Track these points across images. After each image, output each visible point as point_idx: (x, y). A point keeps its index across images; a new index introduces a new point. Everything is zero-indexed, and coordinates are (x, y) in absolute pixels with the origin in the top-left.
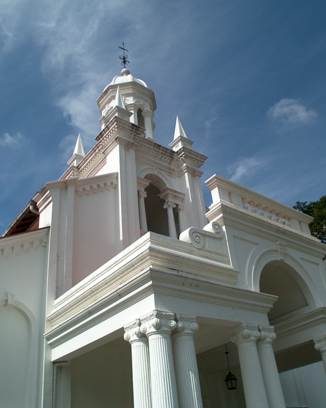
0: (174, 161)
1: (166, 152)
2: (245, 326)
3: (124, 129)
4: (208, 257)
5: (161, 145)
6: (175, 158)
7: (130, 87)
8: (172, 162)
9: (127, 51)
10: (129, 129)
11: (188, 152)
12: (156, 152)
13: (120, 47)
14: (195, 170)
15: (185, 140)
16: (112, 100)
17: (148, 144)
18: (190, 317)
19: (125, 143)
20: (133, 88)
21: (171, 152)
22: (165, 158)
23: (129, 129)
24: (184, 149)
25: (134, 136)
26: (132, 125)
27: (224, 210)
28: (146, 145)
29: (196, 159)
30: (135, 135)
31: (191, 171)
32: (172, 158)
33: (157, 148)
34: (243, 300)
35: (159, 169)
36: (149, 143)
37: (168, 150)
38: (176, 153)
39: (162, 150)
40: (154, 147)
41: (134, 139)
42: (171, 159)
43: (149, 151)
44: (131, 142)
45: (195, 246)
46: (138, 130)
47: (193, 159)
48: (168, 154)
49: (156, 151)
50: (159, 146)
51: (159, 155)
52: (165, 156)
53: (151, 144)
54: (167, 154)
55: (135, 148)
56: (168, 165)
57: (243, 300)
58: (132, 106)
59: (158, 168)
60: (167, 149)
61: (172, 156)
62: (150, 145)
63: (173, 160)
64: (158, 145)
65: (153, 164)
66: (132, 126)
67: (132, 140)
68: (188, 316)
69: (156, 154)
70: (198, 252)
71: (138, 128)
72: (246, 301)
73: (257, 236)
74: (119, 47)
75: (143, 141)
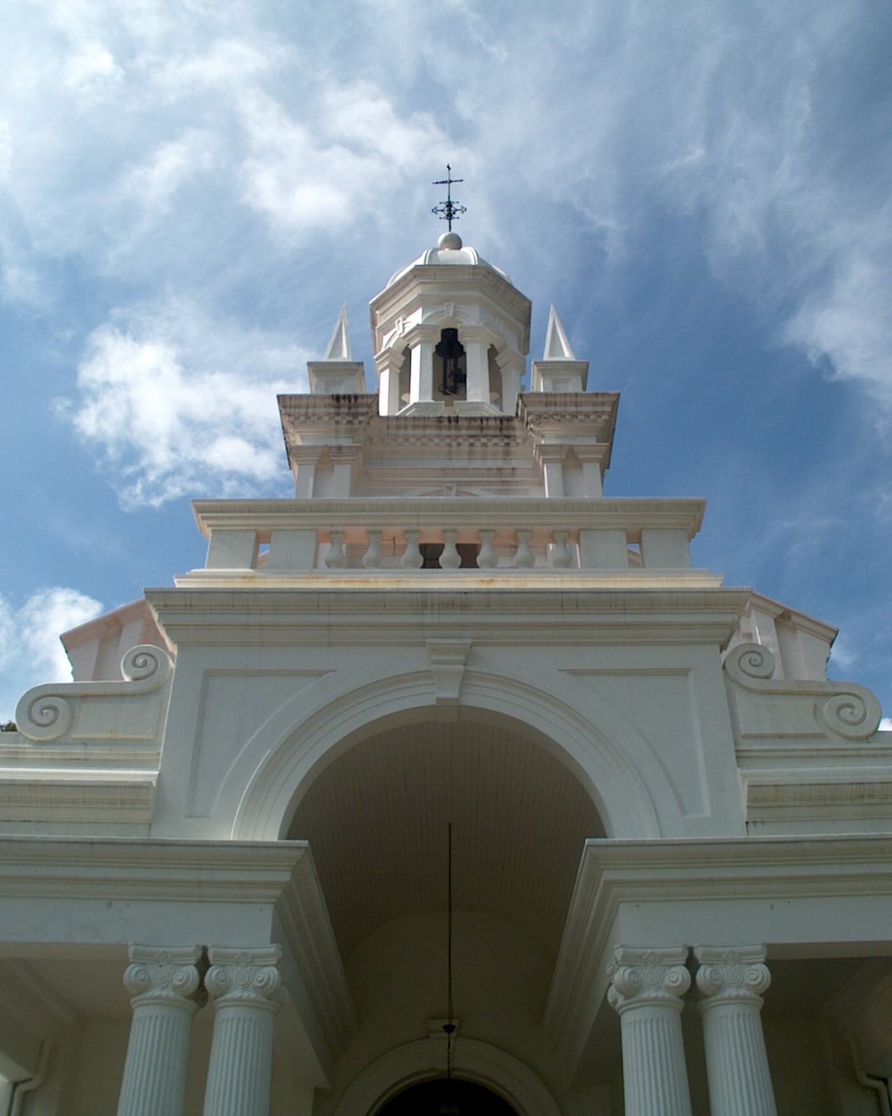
0: (518, 444)
1: (482, 429)
2: (619, 958)
3: (312, 418)
4: (78, 759)
5: (460, 415)
6: (518, 433)
7: (412, 285)
8: (513, 449)
9: (461, 181)
10: (328, 414)
11: (540, 402)
12: (447, 441)
13: (437, 183)
14: (575, 448)
15: (556, 367)
16: (382, 338)
17: (414, 427)
18: (659, 951)
19: (316, 456)
20: (421, 283)
21: (498, 423)
22: (485, 445)
23: (328, 414)
24: (525, 399)
25: (349, 426)
26: (333, 399)
27: (162, 603)
28: (410, 432)
29: (577, 412)
30: (350, 422)
31: (558, 457)
32: (508, 437)
33: (450, 428)
34: (143, 874)
35: (458, 486)
36: (417, 423)
37: (488, 419)
38: (515, 419)
39: (469, 428)
40: (440, 428)
41: (352, 433)
42: (506, 440)
43: (423, 444)
44: (335, 447)
45: (30, 737)
46: (356, 406)
47: (568, 417)
48: (491, 432)
49: (449, 437)
50: (452, 419)
51: (459, 444)
52: (484, 440)
53: (426, 423)
54: (485, 432)
55: (351, 456)
56: (500, 464)
57: (143, 874)
58: (416, 335)
59: (455, 484)
60: (482, 419)
61: (504, 432)
62: (425, 427)
63: (513, 443)
64: (449, 419)
65: (441, 479)
66: (335, 403)
67: (346, 437)
68: (654, 950)
69: (450, 445)
70: (38, 753)
71: (353, 400)
72: (114, 873)
73: (330, 644)
74: (434, 183)
75: (398, 427)
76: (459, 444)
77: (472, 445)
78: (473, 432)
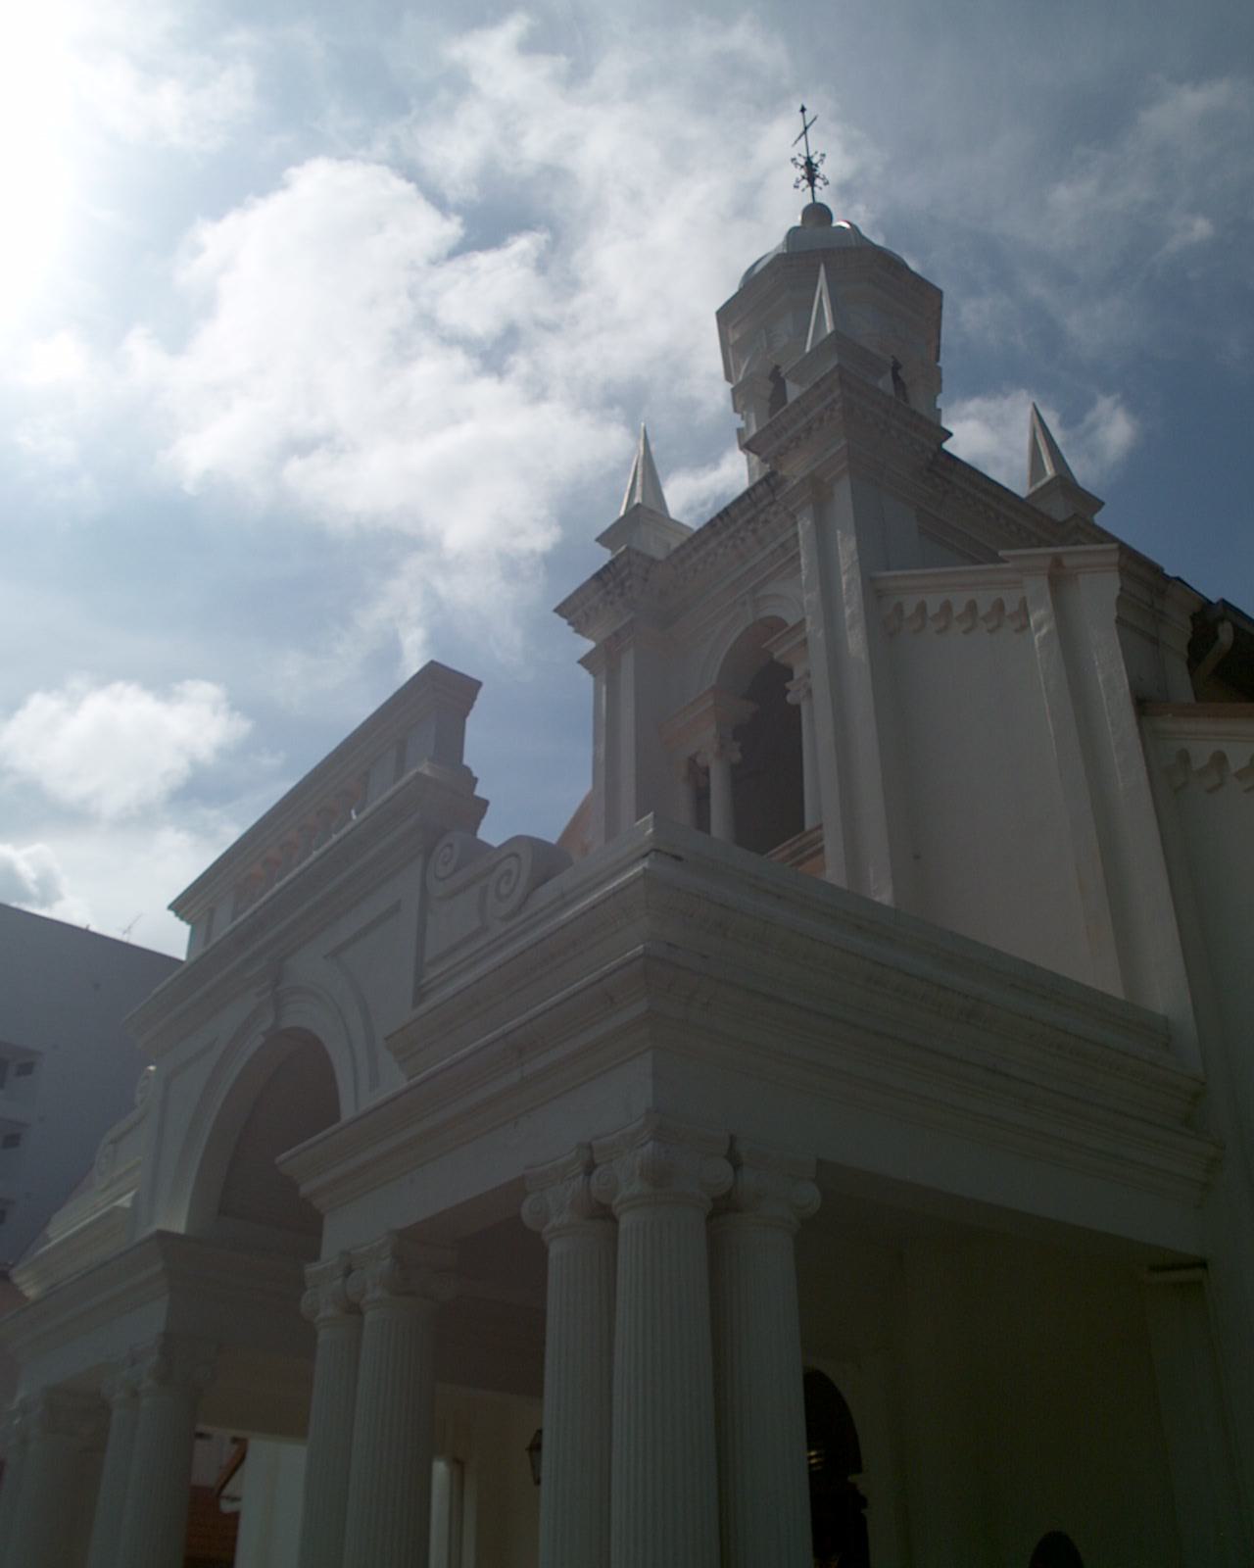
22: (766, 521)
51: (743, 539)
76: (743, 539)
77: (754, 531)
78: (749, 515)
